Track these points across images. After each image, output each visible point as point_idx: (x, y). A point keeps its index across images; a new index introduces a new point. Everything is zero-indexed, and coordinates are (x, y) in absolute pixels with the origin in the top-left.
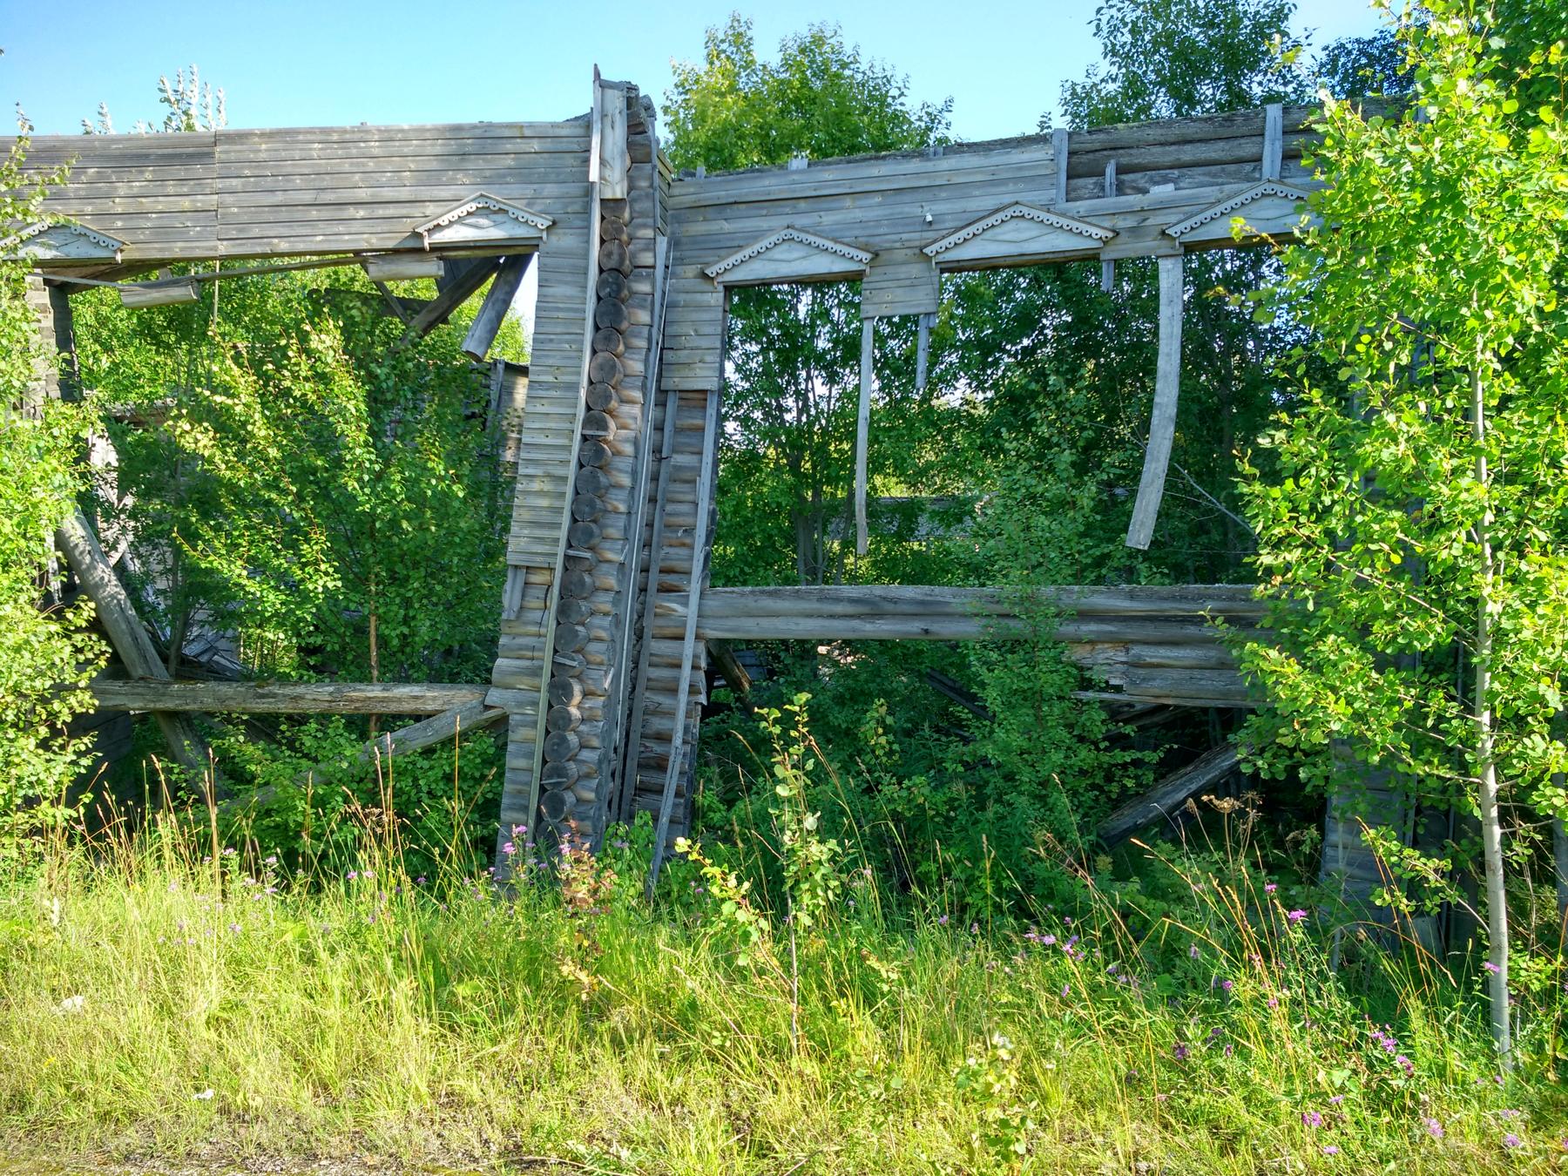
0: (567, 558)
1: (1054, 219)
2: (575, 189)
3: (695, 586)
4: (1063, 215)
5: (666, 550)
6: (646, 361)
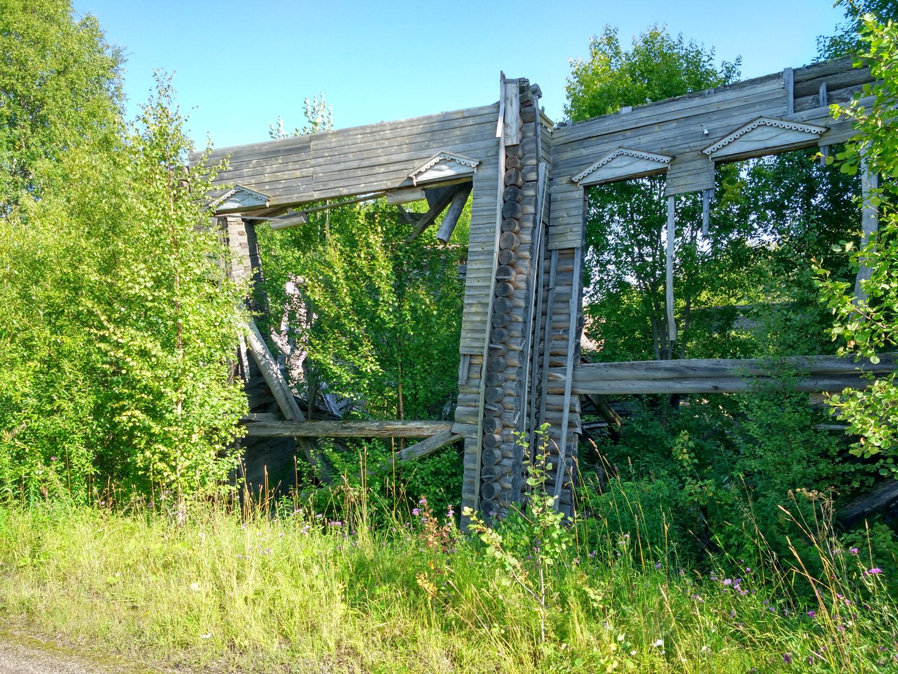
0: (490, 349)
1: (785, 124)
2: (491, 143)
3: (570, 364)
4: (791, 121)
5: (554, 342)
6: (533, 234)
